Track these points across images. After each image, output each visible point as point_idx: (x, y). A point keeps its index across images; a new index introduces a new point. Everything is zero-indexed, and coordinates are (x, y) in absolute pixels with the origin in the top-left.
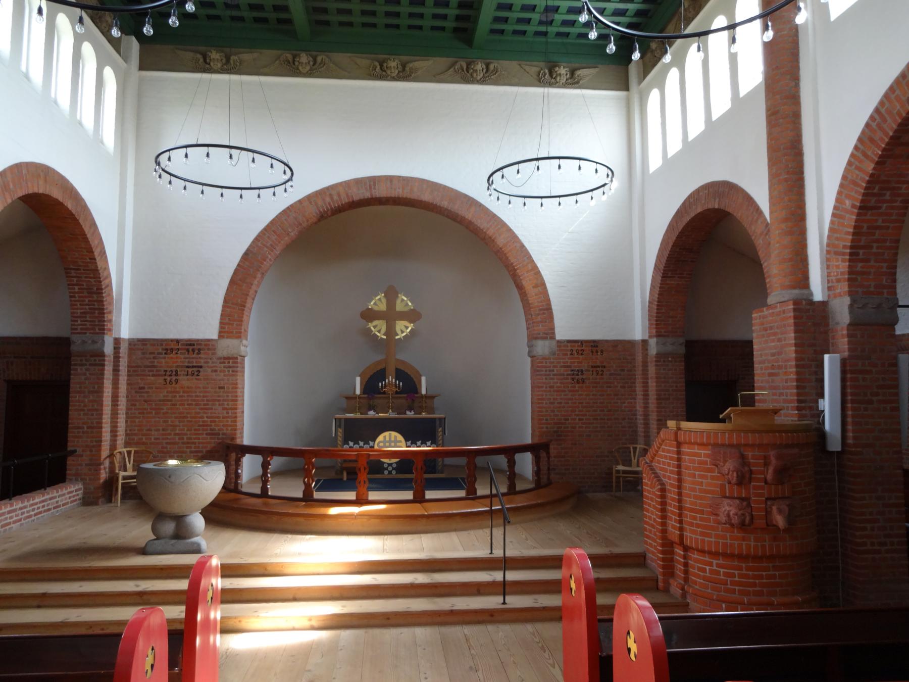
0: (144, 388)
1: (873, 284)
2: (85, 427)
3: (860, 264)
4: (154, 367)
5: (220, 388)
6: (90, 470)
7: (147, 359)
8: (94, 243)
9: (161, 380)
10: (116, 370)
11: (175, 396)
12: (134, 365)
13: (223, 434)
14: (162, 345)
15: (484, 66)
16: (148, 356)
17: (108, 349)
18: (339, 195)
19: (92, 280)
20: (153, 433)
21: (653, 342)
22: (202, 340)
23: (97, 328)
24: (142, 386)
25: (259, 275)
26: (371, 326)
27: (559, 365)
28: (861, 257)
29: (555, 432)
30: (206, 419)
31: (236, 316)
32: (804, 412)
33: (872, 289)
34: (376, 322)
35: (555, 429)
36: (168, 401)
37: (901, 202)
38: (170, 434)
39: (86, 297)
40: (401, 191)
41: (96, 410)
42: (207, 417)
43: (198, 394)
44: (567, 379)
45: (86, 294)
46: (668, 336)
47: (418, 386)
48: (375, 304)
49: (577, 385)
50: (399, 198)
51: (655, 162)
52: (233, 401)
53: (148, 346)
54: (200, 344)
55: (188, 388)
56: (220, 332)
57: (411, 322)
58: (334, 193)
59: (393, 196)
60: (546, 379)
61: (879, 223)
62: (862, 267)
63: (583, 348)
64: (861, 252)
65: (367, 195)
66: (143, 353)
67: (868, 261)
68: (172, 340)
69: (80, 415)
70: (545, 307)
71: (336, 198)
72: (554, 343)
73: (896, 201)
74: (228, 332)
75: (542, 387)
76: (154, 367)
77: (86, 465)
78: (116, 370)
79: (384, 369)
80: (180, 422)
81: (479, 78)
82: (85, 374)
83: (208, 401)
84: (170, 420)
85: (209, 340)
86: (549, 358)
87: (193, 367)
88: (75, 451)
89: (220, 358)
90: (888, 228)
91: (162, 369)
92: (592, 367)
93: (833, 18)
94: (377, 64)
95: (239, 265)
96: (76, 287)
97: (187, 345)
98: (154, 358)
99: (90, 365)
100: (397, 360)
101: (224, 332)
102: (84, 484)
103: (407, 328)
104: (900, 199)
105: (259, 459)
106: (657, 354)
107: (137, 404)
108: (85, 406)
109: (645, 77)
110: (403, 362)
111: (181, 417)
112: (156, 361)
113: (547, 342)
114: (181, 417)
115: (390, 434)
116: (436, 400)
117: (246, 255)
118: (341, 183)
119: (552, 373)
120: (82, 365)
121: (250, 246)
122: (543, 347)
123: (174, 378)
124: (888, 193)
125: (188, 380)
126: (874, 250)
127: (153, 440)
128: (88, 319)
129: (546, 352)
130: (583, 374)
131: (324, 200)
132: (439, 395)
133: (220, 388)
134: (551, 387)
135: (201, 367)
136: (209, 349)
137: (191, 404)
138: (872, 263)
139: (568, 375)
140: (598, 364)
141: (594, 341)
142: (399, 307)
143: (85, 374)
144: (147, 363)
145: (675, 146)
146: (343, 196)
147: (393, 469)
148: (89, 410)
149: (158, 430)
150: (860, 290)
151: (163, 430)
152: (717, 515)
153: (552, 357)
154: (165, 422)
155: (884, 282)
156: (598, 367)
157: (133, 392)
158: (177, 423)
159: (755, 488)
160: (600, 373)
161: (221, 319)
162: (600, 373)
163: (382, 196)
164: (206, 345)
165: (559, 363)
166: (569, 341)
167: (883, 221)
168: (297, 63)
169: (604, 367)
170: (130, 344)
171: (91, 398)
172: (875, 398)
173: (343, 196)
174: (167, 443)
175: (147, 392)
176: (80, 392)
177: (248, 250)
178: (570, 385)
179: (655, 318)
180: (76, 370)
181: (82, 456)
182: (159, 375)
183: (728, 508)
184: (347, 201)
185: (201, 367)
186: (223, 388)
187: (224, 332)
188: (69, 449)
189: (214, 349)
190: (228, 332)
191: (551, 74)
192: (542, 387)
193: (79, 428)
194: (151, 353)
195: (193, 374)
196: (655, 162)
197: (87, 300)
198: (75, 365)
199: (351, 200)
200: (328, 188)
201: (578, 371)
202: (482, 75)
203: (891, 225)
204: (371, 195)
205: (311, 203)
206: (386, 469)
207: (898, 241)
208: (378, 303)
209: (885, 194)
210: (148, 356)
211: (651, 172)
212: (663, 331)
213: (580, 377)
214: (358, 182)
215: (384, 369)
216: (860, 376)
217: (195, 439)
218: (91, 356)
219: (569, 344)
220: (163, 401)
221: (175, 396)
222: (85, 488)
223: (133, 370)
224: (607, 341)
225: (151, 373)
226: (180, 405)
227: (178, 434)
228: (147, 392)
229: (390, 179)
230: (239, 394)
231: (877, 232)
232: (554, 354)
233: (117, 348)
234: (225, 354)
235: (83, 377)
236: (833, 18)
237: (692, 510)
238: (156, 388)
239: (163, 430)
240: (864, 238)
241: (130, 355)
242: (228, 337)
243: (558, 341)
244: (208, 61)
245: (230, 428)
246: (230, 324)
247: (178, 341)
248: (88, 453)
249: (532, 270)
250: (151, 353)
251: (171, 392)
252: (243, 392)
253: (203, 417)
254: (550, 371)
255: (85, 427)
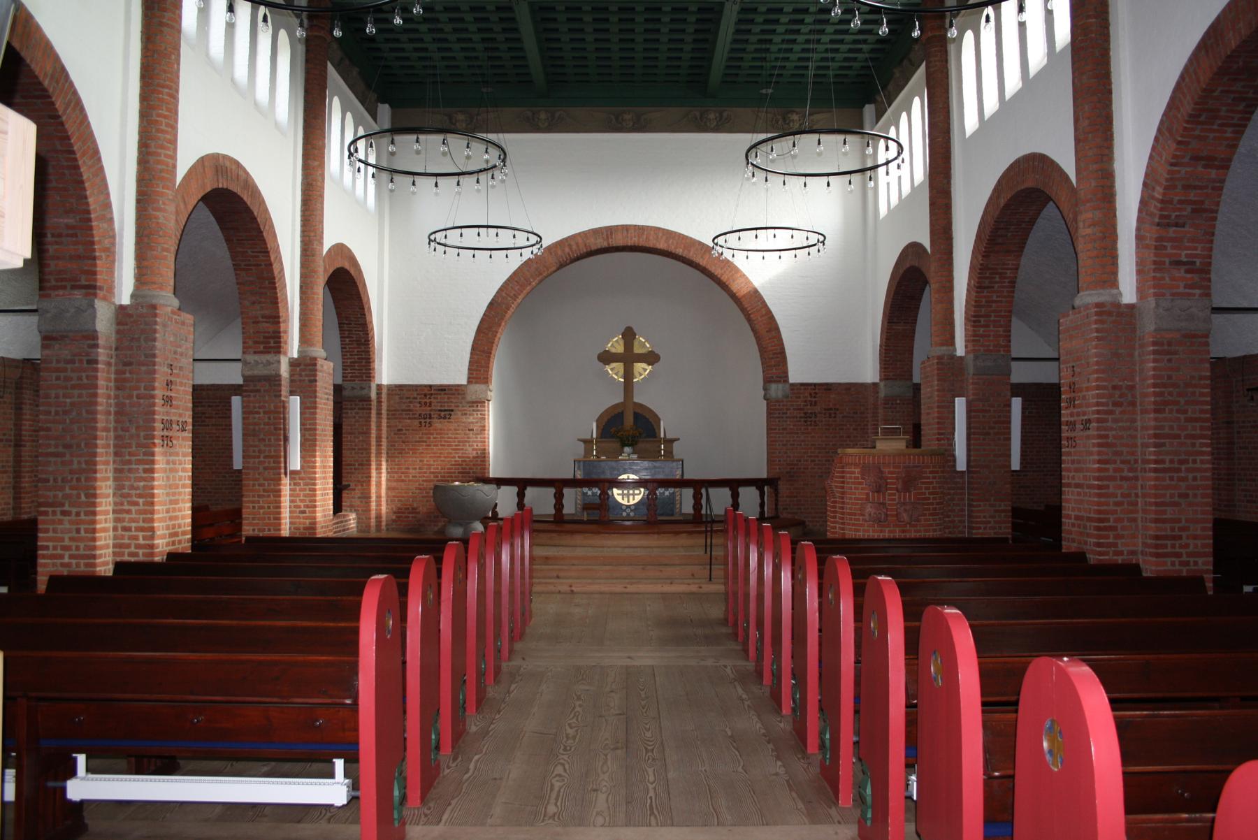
0: (401, 430)
1: (992, 344)
2: (357, 464)
3: (982, 329)
4: (409, 410)
5: (469, 430)
6: (361, 502)
7: (404, 403)
8: (364, 301)
9: (416, 423)
10: (379, 414)
11: (429, 438)
12: (393, 409)
13: (473, 472)
14: (416, 390)
15: (717, 115)
16: (404, 401)
17: (373, 395)
18: (577, 244)
19: (361, 333)
20: (411, 471)
21: (882, 384)
22: (452, 386)
23: (364, 376)
24: (400, 428)
25: (503, 324)
26: (608, 368)
27: (792, 408)
28: (982, 323)
29: (787, 473)
30: (457, 459)
31: (483, 362)
32: (942, 442)
33: (991, 348)
34: (614, 365)
35: (788, 470)
36: (423, 442)
37: (1009, 282)
38: (425, 473)
39: (355, 348)
40: (636, 239)
41: (366, 449)
42: (459, 457)
43: (450, 435)
44: (800, 421)
45: (355, 346)
46: (896, 379)
47: (657, 431)
48: (612, 345)
49: (810, 428)
50: (635, 246)
51: (883, 210)
52: (481, 442)
53: (405, 392)
54: (451, 390)
55: (441, 430)
56: (469, 378)
57: (649, 364)
58: (573, 243)
59: (629, 244)
60: (1171, 479)
61: (995, 298)
62: (984, 331)
63: (817, 391)
64: (982, 319)
65: (605, 244)
66: (401, 398)
67: (988, 326)
68: (425, 386)
69: (351, 454)
70: (779, 351)
71: (574, 247)
72: (787, 386)
73: (1004, 282)
74: (477, 378)
75: (775, 429)
76: (409, 410)
77: (359, 498)
78: (379, 414)
79: (622, 413)
80: (434, 461)
81: (712, 126)
82: (355, 417)
83: (459, 442)
84: (425, 459)
85: (459, 386)
86: (783, 401)
87: (445, 410)
88: (349, 485)
89: (468, 403)
90: (1001, 301)
91: (418, 413)
92: (825, 410)
93: (967, 137)
94: (612, 117)
95: (484, 314)
96: (347, 340)
97: (439, 390)
98: (410, 402)
99: (359, 409)
100: (636, 404)
101: (473, 378)
102: (357, 514)
103: (645, 370)
104: (1007, 280)
105: (514, 490)
106: (885, 397)
107: (396, 444)
108: (356, 445)
109: (877, 122)
110: (642, 406)
111: (435, 457)
112: (412, 405)
113: (780, 386)
114: (435, 457)
115: (628, 502)
116: (675, 444)
117: (491, 305)
118: (579, 234)
119: (784, 416)
120: (351, 409)
121: (495, 296)
122: (777, 390)
123: (428, 420)
124: (997, 276)
125: (440, 422)
126: (992, 318)
127: (411, 478)
128: (357, 368)
129: (780, 395)
130: (816, 416)
131: (563, 250)
132: (678, 439)
133: (469, 430)
134: (784, 429)
135: (452, 411)
136: (459, 394)
137: (444, 445)
138: (992, 328)
139: (801, 417)
140: (831, 406)
141: (827, 384)
142: (637, 350)
143: (355, 417)
144: (404, 407)
145: (894, 201)
146: (582, 246)
147: (631, 510)
148: (359, 449)
149: (415, 469)
150: (982, 349)
151: (420, 468)
152: (864, 515)
153: (785, 400)
154: (421, 461)
155: (1001, 342)
156: (831, 409)
157: (392, 433)
158: (432, 463)
159: (890, 495)
160: (833, 415)
161: (469, 365)
162: (833, 415)
163: (619, 245)
164: (456, 390)
165: (792, 405)
166: (802, 384)
167: (997, 297)
168: (536, 120)
169: (838, 410)
170: (388, 390)
171: (361, 438)
172: (991, 431)
173: (582, 246)
174: (423, 481)
175: (405, 434)
176: (350, 433)
177: (493, 300)
178: (803, 428)
179: (156, 466)
180: (347, 413)
181: (354, 490)
182: (415, 418)
183: (870, 509)
184: (585, 250)
185: (452, 411)
186: (473, 430)
187: (473, 378)
188: (344, 483)
189: (464, 394)
190: (477, 378)
191: (784, 120)
192: (775, 429)
193: (351, 465)
194: (407, 398)
195: (445, 418)
196: (883, 210)
197: (356, 350)
198: (346, 409)
199: (589, 250)
200: (566, 239)
201: (811, 413)
202: (715, 124)
203: (1004, 299)
204: (609, 244)
205: (551, 254)
206: (625, 511)
207: (1010, 311)
208: (616, 345)
209: (995, 278)
210: (404, 401)
211: (881, 218)
212: (891, 374)
213: (813, 419)
214: (596, 232)
215: (622, 413)
216: (981, 414)
217: (448, 477)
218: (361, 401)
219: (802, 387)
220: (419, 442)
221: (429, 438)
222: (359, 518)
223: (392, 413)
224: (840, 384)
225: (408, 417)
226: (435, 446)
227: (433, 473)
228: (405, 434)
229: (626, 228)
230: (486, 436)
231: (994, 305)
232: (787, 397)
233: (379, 394)
234: (474, 398)
235: (354, 420)
236: (967, 137)
237: (850, 514)
238: (413, 430)
239: (420, 468)
240: (983, 310)
241: (388, 401)
242: (476, 383)
243: (792, 385)
244: (454, 121)
245: (479, 468)
246: (477, 370)
247: (430, 386)
248: (360, 487)
249: (766, 314)
250: (407, 398)
251: (426, 434)
252: (488, 434)
253: (455, 457)
254: (783, 413)
255: (357, 464)
